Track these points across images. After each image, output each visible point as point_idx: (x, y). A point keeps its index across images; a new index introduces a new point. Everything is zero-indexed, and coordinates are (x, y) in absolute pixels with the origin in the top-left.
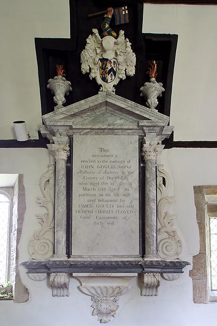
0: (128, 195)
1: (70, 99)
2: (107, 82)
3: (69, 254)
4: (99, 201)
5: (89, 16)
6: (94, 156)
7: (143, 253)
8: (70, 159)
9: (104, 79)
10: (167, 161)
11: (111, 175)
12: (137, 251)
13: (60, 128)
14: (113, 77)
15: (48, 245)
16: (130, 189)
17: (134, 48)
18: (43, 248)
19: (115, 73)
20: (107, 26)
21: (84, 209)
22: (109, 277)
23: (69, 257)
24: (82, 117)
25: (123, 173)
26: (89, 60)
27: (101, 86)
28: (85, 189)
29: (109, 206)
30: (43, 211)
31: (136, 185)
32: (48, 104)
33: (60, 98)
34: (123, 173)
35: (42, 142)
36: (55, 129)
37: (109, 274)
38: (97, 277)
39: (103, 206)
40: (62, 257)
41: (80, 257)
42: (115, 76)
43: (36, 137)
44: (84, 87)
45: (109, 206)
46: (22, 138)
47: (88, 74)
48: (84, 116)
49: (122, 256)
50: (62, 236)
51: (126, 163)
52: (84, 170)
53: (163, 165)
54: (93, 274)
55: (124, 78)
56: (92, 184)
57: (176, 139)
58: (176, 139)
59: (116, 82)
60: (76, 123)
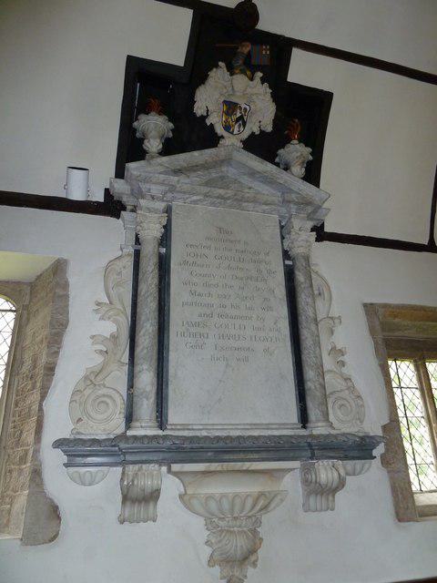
0: (270, 309)
1: (169, 148)
2: (232, 133)
3: (161, 420)
4: (220, 316)
5: (217, 45)
6: (208, 238)
7: (304, 419)
8: (165, 240)
9: (227, 128)
10: (328, 262)
11: (240, 274)
12: (294, 417)
13: (153, 187)
14: (242, 129)
15: (110, 397)
16: (272, 299)
17: (275, 97)
18: (103, 407)
19: (244, 124)
20: (241, 62)
21: (193, 330)
22: (247, 471)
23: (162, 425)
24: (189, 177)
25: (259, 271)
26: (208, 100)
27: (222, 137)
28: (193, 293)
29: (237, 326)
30: (108, 328)
31: (281, 291)
32: (130, 148)
33: (153, 145)
34: (259, 271)
35: (111, 206)
36: (144, 187)
37: (247, 465)
38: (220, 472)
39: (227, 326)
40: (145, 427)
41: (185, 427)
42: (244, 126)
43: (99, 197)
44: (192, 135)
45: (237, 326)
46: (77, 195)
47: (203, 118)
48: (193, 174)
49: (268, 426)
50: (146, 379)
51: (262, 256)
52: (191, 260)
53: (317, 265)
54: (214, 466)
55: (257, 133)
56: (206, 285)
57: (328, 229)
58: (328, 229)
59: (245, 135)
60: (182, 182)
